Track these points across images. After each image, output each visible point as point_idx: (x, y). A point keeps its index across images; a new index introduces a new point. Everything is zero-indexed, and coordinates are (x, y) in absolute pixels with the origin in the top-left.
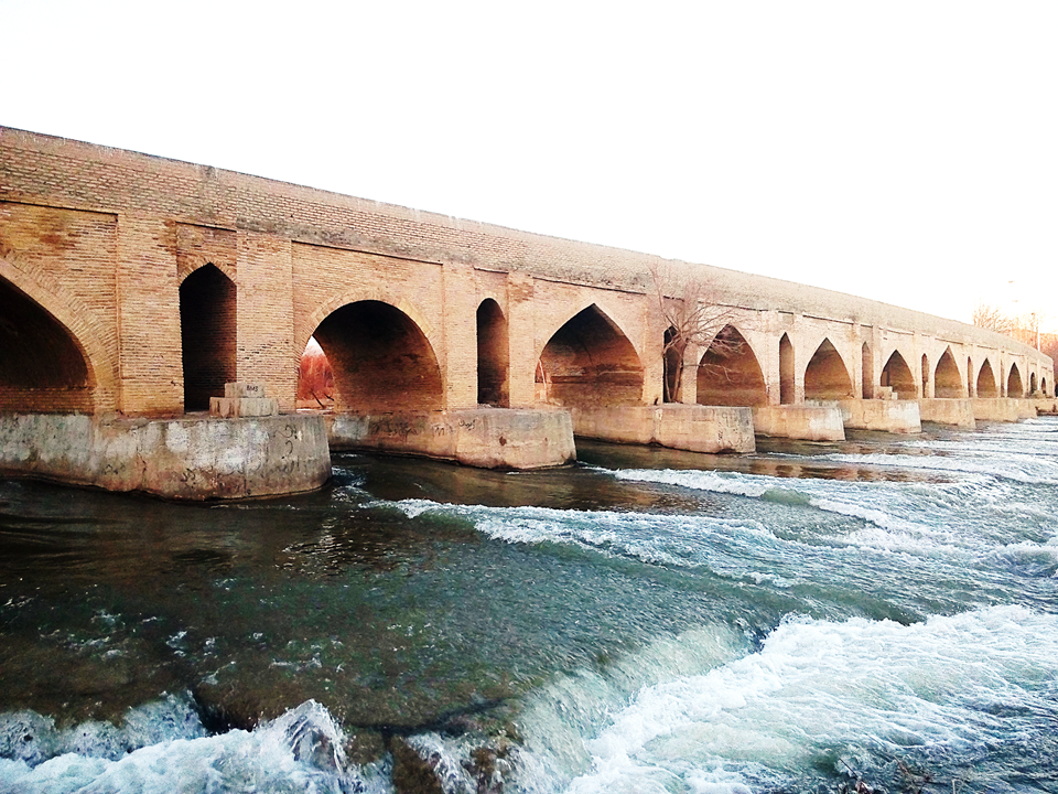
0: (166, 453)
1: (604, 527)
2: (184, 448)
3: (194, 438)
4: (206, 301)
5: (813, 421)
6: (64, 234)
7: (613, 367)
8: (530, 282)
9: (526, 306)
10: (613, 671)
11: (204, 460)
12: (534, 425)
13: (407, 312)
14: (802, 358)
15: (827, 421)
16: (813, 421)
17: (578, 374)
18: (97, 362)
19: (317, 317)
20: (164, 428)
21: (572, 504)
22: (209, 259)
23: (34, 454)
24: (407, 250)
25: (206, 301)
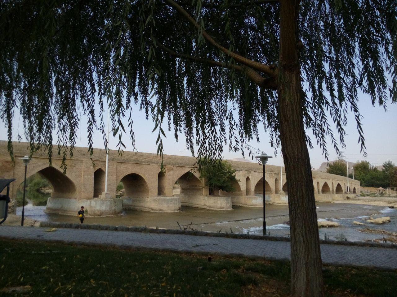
0: (91, 206)
1: (27, 288)
2: (94, 205)
3: (96, 204)
4: (99, 175)
5: (253, 200)
6: (74, 164)
7: (196, 186)
8: (172, 167)
9: (171, 173)
10: (328, 167)
11: (98, 208)
12: (170, 201)
13: (141, 175)
14: (335, 186)
15: (257, 201)
16: (253, 200)
17: (188, 187)
18: (77, 189)
19: (121, 177)
20: (91, 202)
21: (340, 174)
22: (100, 167)
23: (62, 206)
24: (142, 162)
25: (99, 175)
